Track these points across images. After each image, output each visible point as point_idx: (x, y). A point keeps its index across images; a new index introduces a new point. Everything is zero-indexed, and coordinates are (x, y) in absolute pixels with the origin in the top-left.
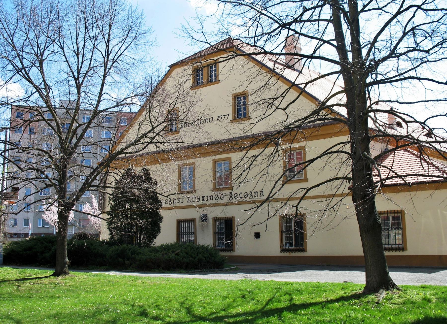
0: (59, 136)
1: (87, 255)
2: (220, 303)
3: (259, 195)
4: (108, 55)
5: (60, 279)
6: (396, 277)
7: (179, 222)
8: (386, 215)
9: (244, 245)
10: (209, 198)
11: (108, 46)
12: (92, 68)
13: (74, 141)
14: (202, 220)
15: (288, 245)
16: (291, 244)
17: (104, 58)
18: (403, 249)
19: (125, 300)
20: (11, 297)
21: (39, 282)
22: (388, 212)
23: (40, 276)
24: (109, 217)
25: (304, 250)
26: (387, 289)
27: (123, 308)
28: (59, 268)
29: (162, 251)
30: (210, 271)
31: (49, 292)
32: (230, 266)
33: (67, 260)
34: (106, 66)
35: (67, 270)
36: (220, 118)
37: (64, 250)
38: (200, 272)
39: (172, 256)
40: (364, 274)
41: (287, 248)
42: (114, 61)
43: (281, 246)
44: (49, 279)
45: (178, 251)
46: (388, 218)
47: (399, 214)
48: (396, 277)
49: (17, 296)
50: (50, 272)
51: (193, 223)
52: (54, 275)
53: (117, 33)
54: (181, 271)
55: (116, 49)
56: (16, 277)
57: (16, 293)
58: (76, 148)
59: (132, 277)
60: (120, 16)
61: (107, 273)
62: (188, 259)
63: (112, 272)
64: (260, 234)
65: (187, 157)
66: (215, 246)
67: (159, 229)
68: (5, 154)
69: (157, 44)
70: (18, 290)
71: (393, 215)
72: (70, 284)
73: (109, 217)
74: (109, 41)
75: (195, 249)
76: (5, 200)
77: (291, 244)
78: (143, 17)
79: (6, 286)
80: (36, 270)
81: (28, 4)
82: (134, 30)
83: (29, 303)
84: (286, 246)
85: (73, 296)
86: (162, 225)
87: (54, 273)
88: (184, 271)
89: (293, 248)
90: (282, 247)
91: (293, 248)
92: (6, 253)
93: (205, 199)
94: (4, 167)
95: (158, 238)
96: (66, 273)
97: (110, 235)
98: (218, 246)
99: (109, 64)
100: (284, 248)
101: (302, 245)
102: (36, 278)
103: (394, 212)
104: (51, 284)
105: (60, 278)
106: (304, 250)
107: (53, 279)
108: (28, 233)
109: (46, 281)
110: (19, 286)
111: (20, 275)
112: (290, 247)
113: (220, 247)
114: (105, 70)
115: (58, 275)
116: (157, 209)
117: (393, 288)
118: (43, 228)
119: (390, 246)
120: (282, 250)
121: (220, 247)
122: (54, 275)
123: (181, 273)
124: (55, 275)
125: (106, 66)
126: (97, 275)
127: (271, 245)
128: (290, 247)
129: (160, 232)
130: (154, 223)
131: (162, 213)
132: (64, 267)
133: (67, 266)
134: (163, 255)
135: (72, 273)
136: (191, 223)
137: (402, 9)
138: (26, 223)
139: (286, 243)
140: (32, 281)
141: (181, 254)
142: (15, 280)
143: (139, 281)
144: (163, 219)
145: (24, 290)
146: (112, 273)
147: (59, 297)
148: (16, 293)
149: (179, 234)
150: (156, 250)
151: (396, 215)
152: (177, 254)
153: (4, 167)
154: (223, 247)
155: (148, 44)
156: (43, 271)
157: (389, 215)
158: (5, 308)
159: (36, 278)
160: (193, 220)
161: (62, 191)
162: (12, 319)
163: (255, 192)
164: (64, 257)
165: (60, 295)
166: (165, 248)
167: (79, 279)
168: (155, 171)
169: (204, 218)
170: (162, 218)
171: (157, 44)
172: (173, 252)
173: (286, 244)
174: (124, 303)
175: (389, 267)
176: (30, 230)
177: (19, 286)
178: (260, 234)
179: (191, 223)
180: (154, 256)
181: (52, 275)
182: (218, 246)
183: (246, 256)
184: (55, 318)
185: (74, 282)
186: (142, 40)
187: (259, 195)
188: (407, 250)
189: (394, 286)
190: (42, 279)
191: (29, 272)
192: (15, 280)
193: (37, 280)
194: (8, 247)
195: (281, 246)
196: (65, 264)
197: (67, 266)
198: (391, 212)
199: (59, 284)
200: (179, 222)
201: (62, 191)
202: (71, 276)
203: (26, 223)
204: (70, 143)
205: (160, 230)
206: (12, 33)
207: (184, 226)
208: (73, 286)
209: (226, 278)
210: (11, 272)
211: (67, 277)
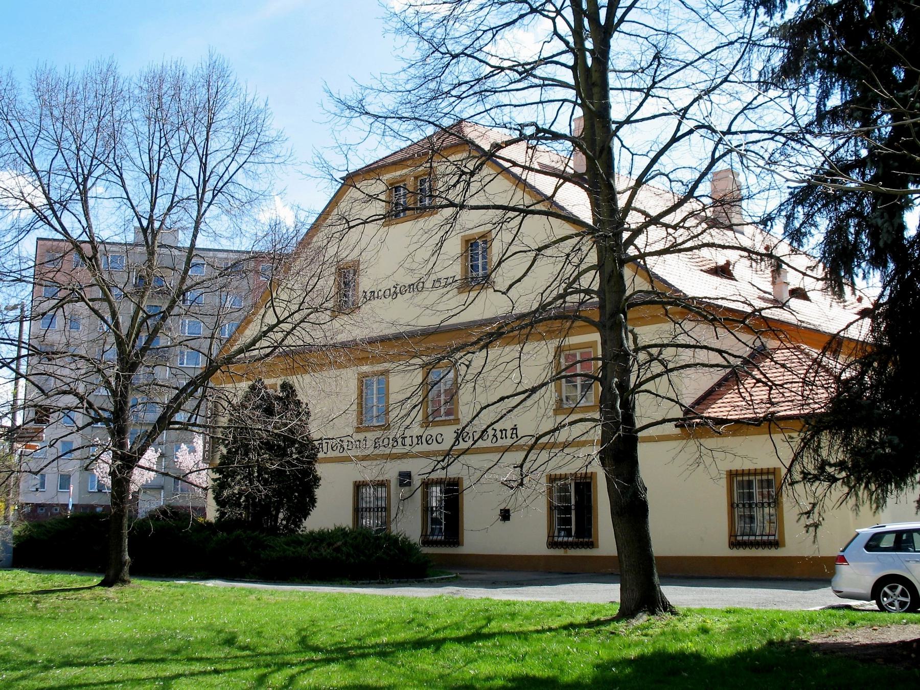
0: (125, 311)
1: (173, 548)
2: (360, 630)
3: (509, 435)
4: (205, 182)
5: (112, 592)
6: (672, 593)
7: (358, 487)
8: (746, 478)
9: (480, 534)
10: (415, 440)
11: (205, 164)
12: (178, 202)
13: (144, 336)
14: (402, 484)
15: (562, 533)
16: (569, 534)
17: (197, 188)
18: (776, 544)
19: (211, 624)
20: (20, 617)
21: (74, 597)
22: (749, 473)
23: (78, 586)
24: (217, 476)
25: (591, 545)
26: (653, 613)
27: (203, 635)
28: (112, 573)
29: (308, 544)
30: (398, 582)
31: (87, 612)
32: (443, 573)
33: (127, 557)
34: (200, 202)
35: (127, 577)
36: (437, 285)
37: (121, 540)
38: (379, 583)
39: (325, 551)
40: (618, 586)
41: (560, 539)
42: (217, 191)
43: (730, 536)
44: (92, 591)
45: (339, 543)
46: (750, 483)
47: (771, 477)
48: (672, 593)
49: (32, 617)
50: (97, 580)
51: (384, 489)
52: (103, 584)
53: (221, 142)
54: (344, 581)
55: (221, 169)
56: (34, 588)
57: (32, 612)
58: (143, 356)
59: (243, 589)
60: (229, 108)
61: (202, 583)
62: (367, 557)
63: (213, 582)
64: (507, 512)
65: (376, 360)
66: (426, 535)
67: (313, 501)
68: (18, 366)
69: (294, 162)
70: (35, 607)
71: (740, 478)
72: (129, 600)
73: (217, 476)
74: (207, 155)
75: (372, 541)
76: (18, 442)
77: (569, 534)
78: (269, 112)
79: (15, 602)
80: (74, 576)
81: (13, 330)
82: (251, 137)
83: (50, 627)
84: (559, 536)
85: (127, 618)
86: (318, 492)
87: (103, 581)
88: (348, 582)
89: (570, 539)
90: (551, 539)
91: (570, 539)
92: (18, 545)
93: (408, 441)
94: (16, 384)
95: (309, 518)
96: (124, 582)
97: (218, 510)
98: (433, 534)
99: (208, 196)
100: (556, 539)
101: (590, 536)
102: (69, 590)
103: (762, 472)
104: (95, 599)
105: (112, 589)
106: (591, 545)
107: (100, 591)
108: (67, 505)
109: (87, 594)
110: (37, 602)
111: (42, 585)
112: (566, 539)
113: (435, 537)
114: (199, 211)
115: (110, 585)
116: (310, 463)
117: (665, 610)
118: (99, 494)
119: (765, 538)
120: (552, 544)
121: (435, 537)
122: (103, 584)
123: (342, 585)
124: (105, 584)
125: (200, 202)
126: (182, 586)
127: (530, 533)
128: (566, 539)
129: (314, 506)
130: (300, 489)
131: (320, 469)
132: (121, 570)
133: (126, 568)
134: (310, 550)
135: (135, 582)
136: (380, 489)
137: (679, 134)
138: (65, 482)
139: (560, 530)
140: (62, 594)
141: (344, 549)
142: (32, 593)
143: (253, 597)
144: (321, 482)
145: (46, 608)
146: (211, 583)
147: (102, 619)
148: (32, 612)
149: (358, 511)
150: (298, 542)
151: (765, 477)
152: (338, 550)
153: (16, 384)
154: (439, 538)
155: (277, 161)
156: (85, 578)
157: (752, 478)
158: (8, 632)
159: (69, 590)
160: (382, 484)
161: (119, 433)
162: (19, 646)
163: (501, 431)
164: (120, 552)
165: (106, 616)
166: (321, 538)
167: (146, 592)
168: (307, 387)
169: (405, 478)
170: (319, 479)
171: (294, 162)
172: (329, 545)
173: (559, 532)
174: (207, 628)
175: (660, 577)
176: (71, 498)
177: (37, 602)
178: (507, 512)
179: (380, 489)
180: (293, 553)
181: (99, 585)
182: (433, 534)
183: (514, 556)
184: (87, 645)
185: (138, 596)
186: (266, 156)
187: (509, 435)
188: (784, 546)
189: (667, 607)
190: (81, 592)
191: (59, 579)
192: (32, 593)
193: (71, 593)
194: (22, 534)
195: (550, 535)
196: (122, 564)
197: (126, 568)
198: (755, 473)
199: (108, 599)
200: (358, 487)
201: (119, 433)
202: (133, 588)
203: (65, 482)
204: (133, 347)
205: (315, 502)
206: (31, 145)
207: (368, 492)
208: (132, 603)
209: (419, 595)
210: (26, 580)
211: (127, 589)
